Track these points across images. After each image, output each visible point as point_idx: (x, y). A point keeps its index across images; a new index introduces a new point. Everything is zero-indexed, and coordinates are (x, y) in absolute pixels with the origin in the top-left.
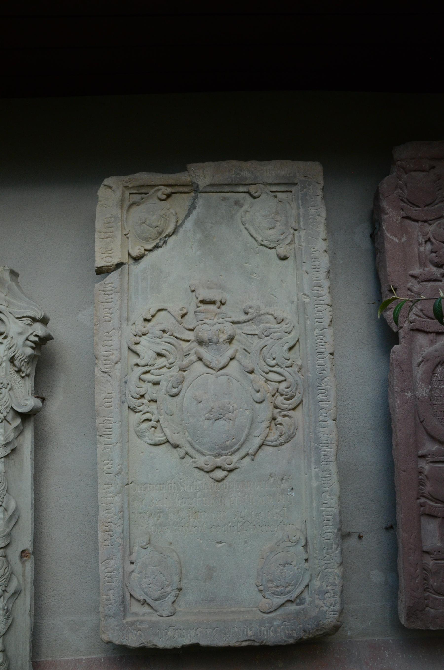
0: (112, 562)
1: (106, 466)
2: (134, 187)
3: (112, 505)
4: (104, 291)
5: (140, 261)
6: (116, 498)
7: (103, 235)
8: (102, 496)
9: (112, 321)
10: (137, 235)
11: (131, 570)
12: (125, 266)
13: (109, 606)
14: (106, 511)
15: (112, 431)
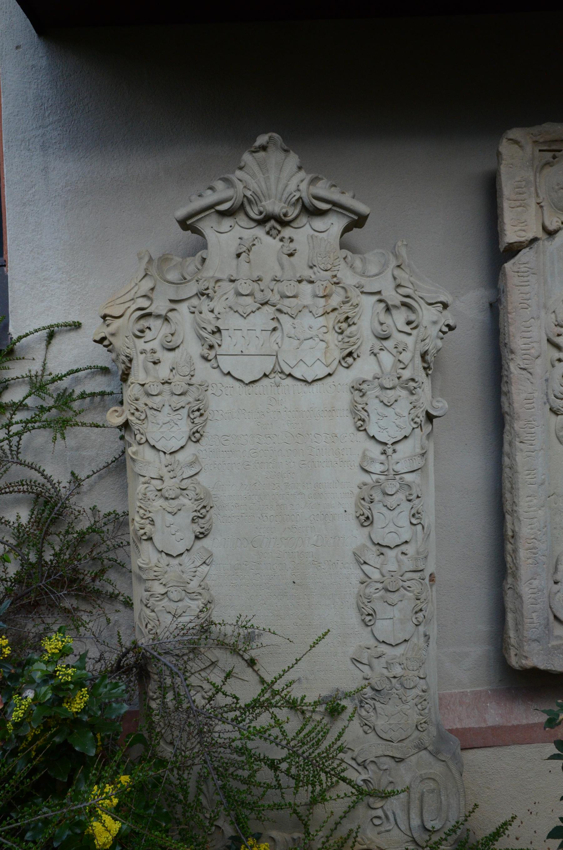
0: (536, 583)
1: (529, 477)
2: (545, 142)
3: (535, 519)
4: (518, 272)
5: (555, 236)
6: (540, 512)
7: (513, 204)
8: (525, 510)
9: (529, 309)
10: (554, 204)
11: (557, 591)
12: (539, 241)
13: (534, 629)
14: (529, 527)
15: (534, 437)
